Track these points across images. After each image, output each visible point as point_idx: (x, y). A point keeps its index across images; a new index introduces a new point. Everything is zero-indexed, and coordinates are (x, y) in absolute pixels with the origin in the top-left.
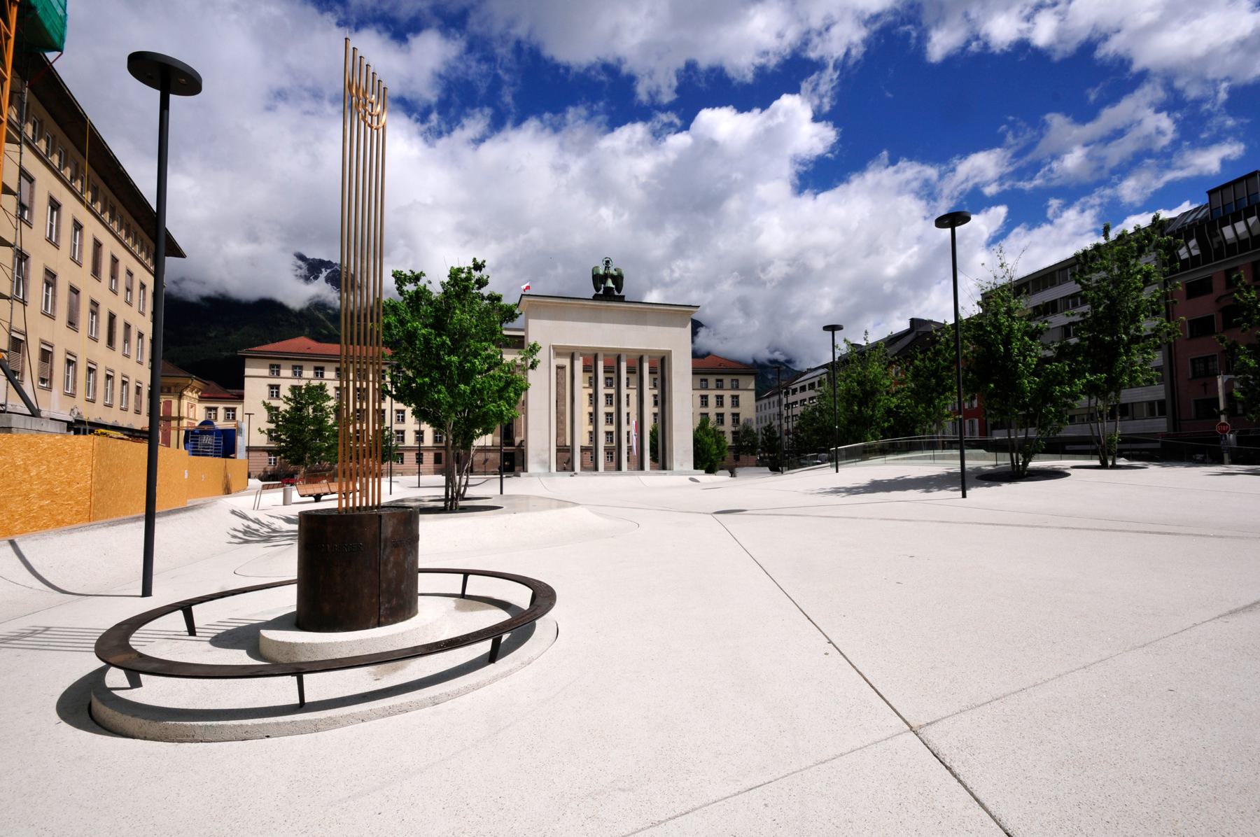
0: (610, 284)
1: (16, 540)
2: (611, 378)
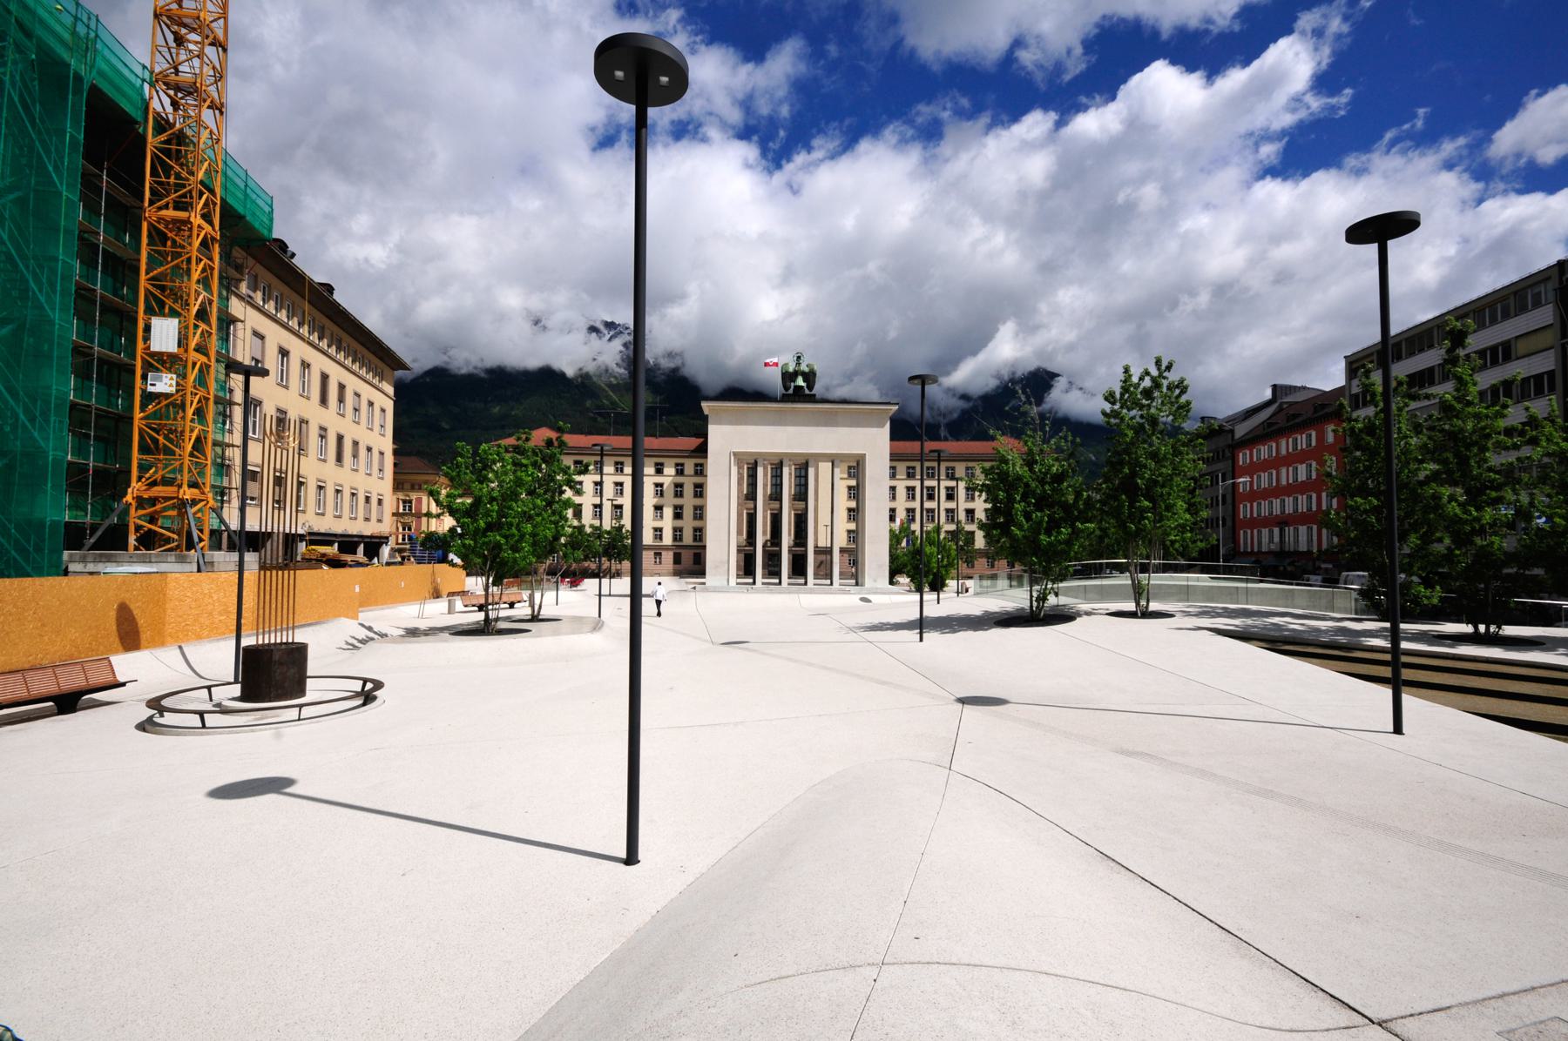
0: (800, 382)
1: (183, 645)
2: (914, 468)
